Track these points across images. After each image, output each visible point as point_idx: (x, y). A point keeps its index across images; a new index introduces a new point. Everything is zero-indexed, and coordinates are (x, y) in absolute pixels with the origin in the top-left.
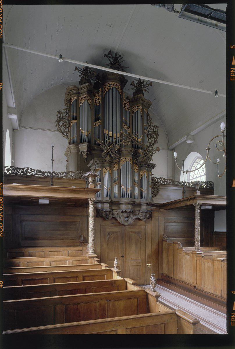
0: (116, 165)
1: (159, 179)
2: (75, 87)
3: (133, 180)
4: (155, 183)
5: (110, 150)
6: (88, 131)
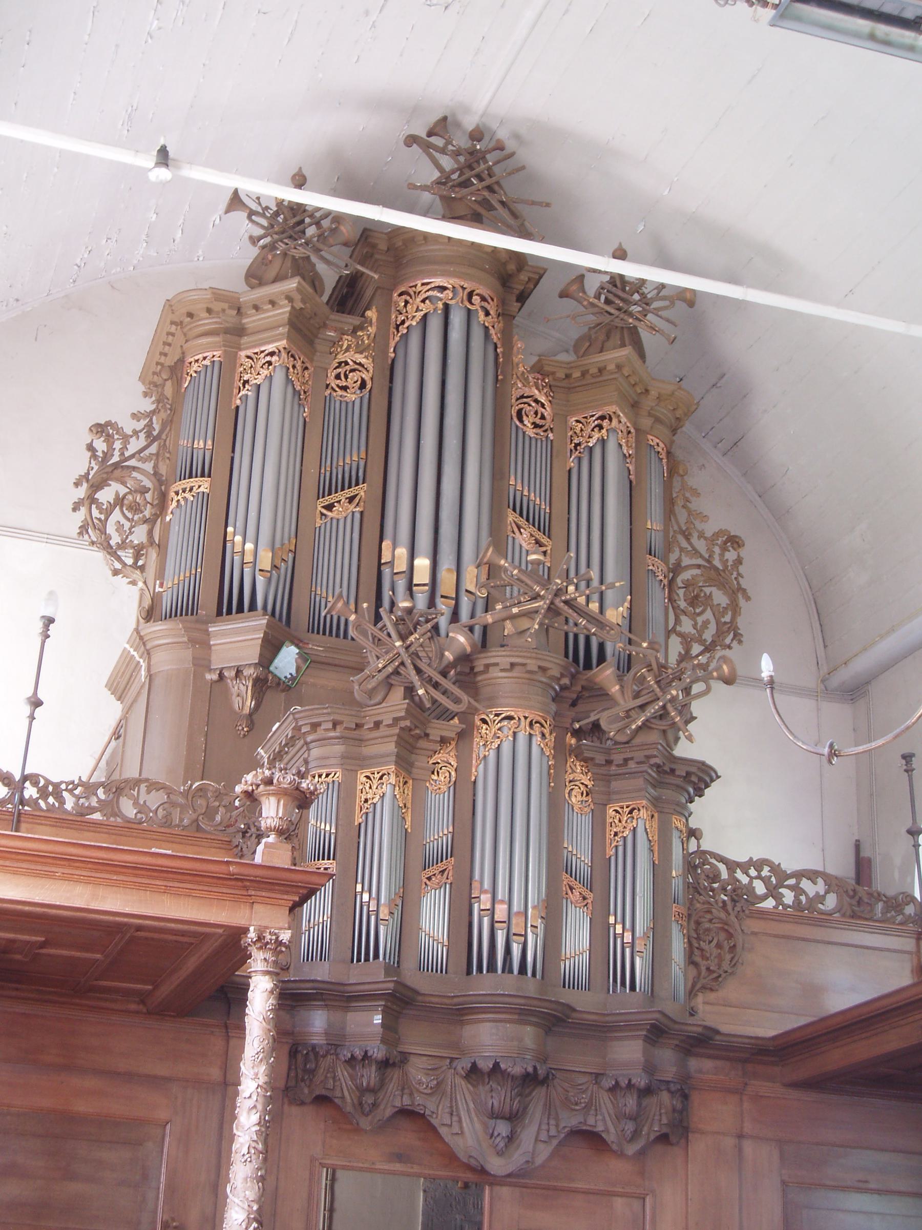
0: (447, 757)
1: (738, 865)
2: (218, 295)
3: (557, 866)
4: (713, 890)
5: (408, 662)
6: (278, 545)
